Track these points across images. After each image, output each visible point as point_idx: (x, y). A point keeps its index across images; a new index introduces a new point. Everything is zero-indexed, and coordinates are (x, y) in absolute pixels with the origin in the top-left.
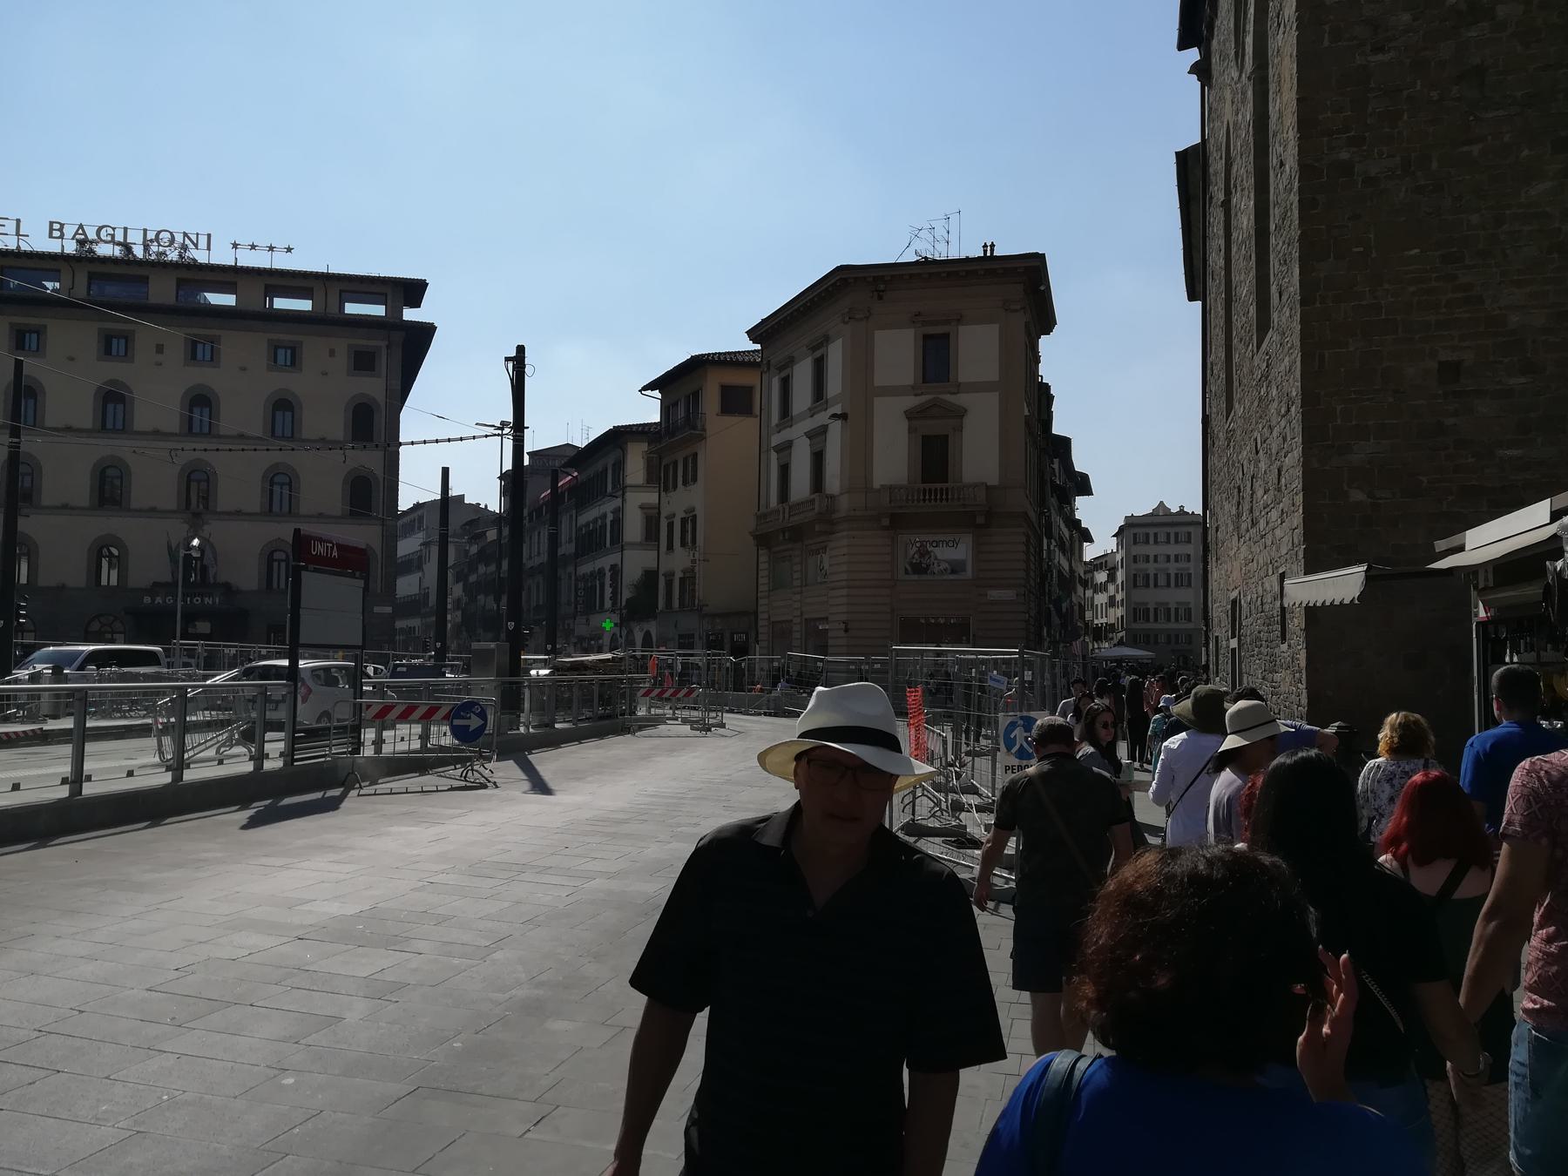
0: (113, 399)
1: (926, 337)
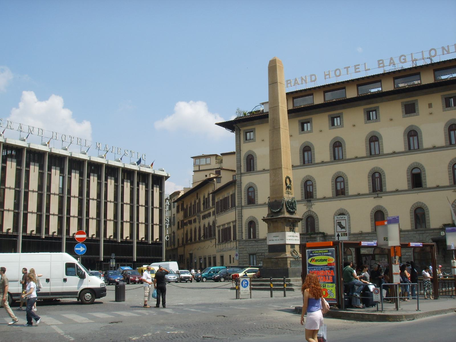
0: (412, 134)
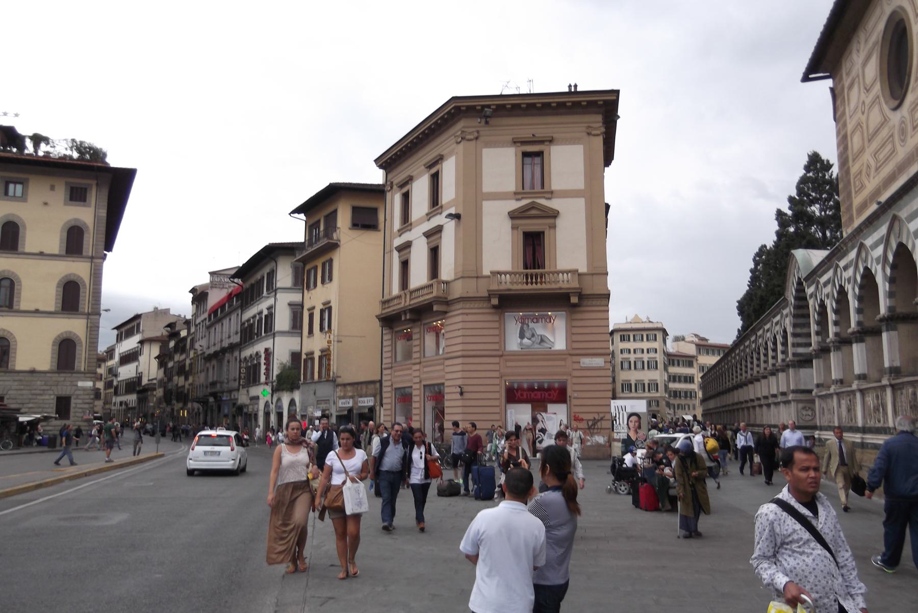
1: (525, 155)
